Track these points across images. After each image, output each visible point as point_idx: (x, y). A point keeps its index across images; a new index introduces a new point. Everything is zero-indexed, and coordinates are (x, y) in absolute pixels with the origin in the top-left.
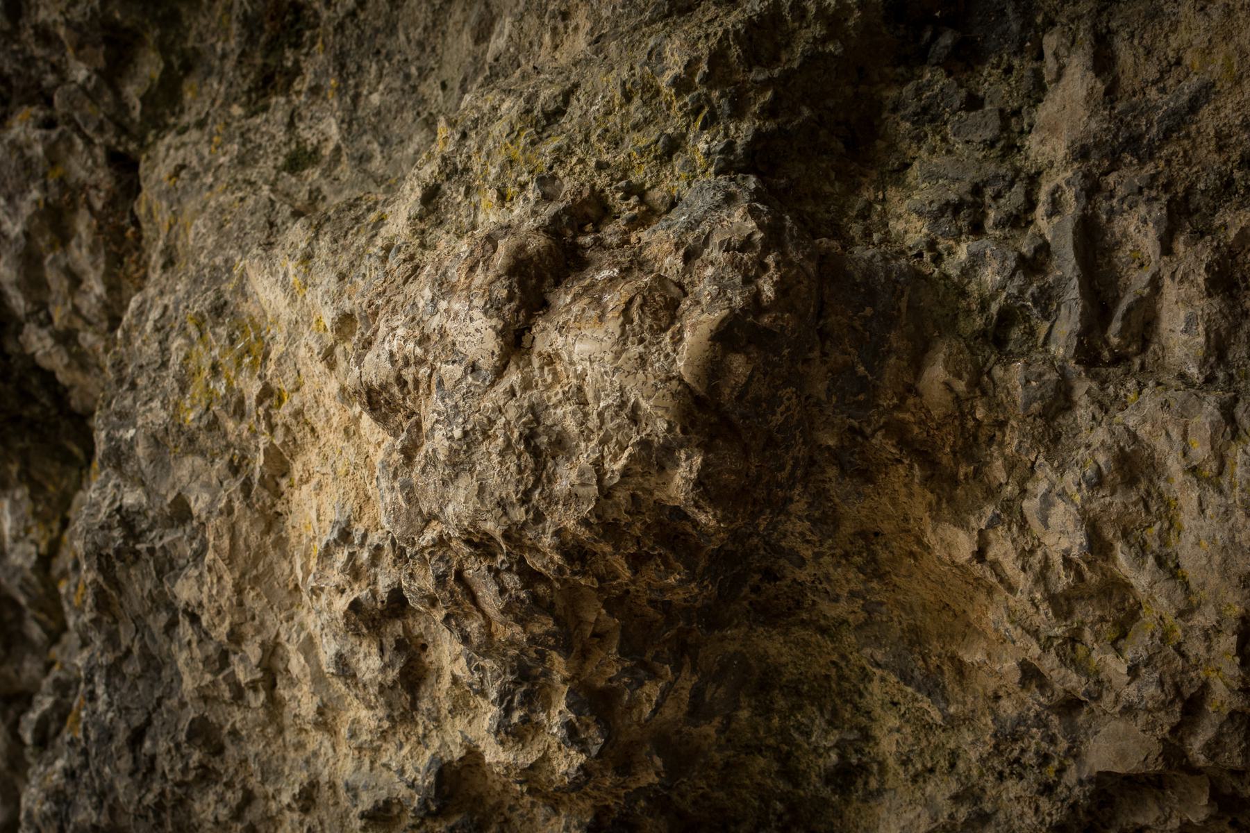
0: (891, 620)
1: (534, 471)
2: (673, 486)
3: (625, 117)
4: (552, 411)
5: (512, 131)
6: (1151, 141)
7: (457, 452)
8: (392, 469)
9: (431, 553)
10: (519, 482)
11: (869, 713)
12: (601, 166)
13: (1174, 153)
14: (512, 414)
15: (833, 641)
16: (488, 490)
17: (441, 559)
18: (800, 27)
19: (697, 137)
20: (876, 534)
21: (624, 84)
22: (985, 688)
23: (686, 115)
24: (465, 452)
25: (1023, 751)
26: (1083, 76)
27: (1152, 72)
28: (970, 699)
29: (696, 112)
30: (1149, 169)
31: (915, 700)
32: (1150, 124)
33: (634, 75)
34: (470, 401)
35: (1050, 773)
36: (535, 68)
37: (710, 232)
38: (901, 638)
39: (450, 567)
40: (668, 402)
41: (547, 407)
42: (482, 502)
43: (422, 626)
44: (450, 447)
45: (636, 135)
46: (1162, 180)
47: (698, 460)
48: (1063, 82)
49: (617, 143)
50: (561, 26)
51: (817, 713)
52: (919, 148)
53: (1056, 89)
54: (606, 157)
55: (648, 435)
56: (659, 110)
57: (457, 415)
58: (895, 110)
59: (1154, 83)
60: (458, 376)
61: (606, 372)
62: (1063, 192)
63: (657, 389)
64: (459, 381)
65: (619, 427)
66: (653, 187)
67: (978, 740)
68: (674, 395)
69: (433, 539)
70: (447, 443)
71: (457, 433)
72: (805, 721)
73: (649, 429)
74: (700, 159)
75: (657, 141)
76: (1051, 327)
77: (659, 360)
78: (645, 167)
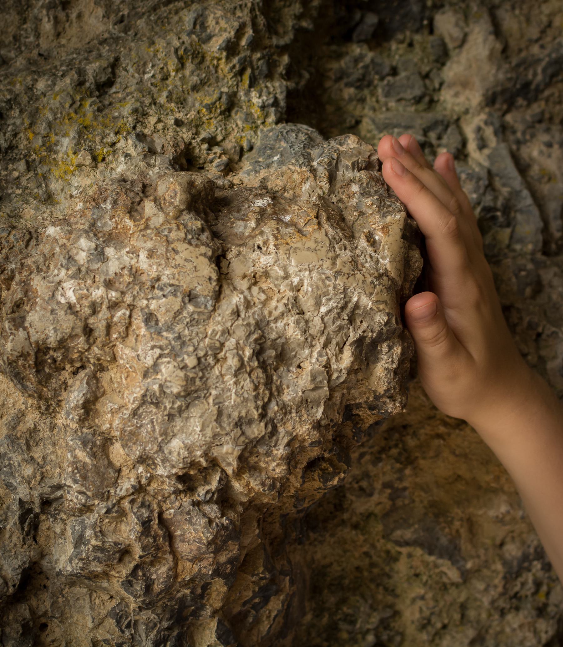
0: (413, 501)
1: (266, 384)
2: (374, 379)
3: (183, 79)
4: (272, 325)
5: (74, 102)
6: (538, 86)
7: (193, 380)
8: (22, 442)
9: (132, 502)
10: (256, 397)
11: (393, 590)
12: (178, 123)
13: (552, 94)
14: (241, 333)
15: (363, 534)
16: (225, 412)
17: (143, 505)
18: (284, 6)
19: (247, 93)
20: (405, 427)
21: (176, 50)
22: (493, 539)
23: (235, 76)
24: (201, 378)
25: (523, 584)
26: (485, 41)
27: (534, 32)
28: (482, 552)
29: (241, 72)
30: (536, 108)
31: (436, 566)
32: (535, 74)
33: (183, 43)
34: (195, 329)
35: (541, 598)
36: (40, 55)
37: (338, 158)
38: (426, 514)
39: (152, 511)
40: (385, 296)
41: (268, 322)
42: (221, 426)
43: (48, 604)
44: (186, 377)
45: (198, 96)
46: (547, 116)
47: (398, 350)
48: (466, 47)
49: (182, 102)
50: (62, 15)
51: (361, 601)
52: (364, 108)
53: (459, 54)
54: (180, 115)
55: (364, 332)
56: (208, 73)
57: (183, 344)
58: (339, 79)
59: (537, 41)
60: (177, 307)
61: (327, 278)
62: (484, 131)
63: (375, 286)
64: (178, 313)
65: (340, 328)
66: (224, 139)
67: (488, 586)
68: (388, 289)
69: (133, 487)
70: (181, 374)
71: (191, 362)
72: (350, 611)
73: (365, 325)
74: (256, 112)
75: (220, 98)
76: (513, 232)
77: (366, 262)
78: (214, 121)
